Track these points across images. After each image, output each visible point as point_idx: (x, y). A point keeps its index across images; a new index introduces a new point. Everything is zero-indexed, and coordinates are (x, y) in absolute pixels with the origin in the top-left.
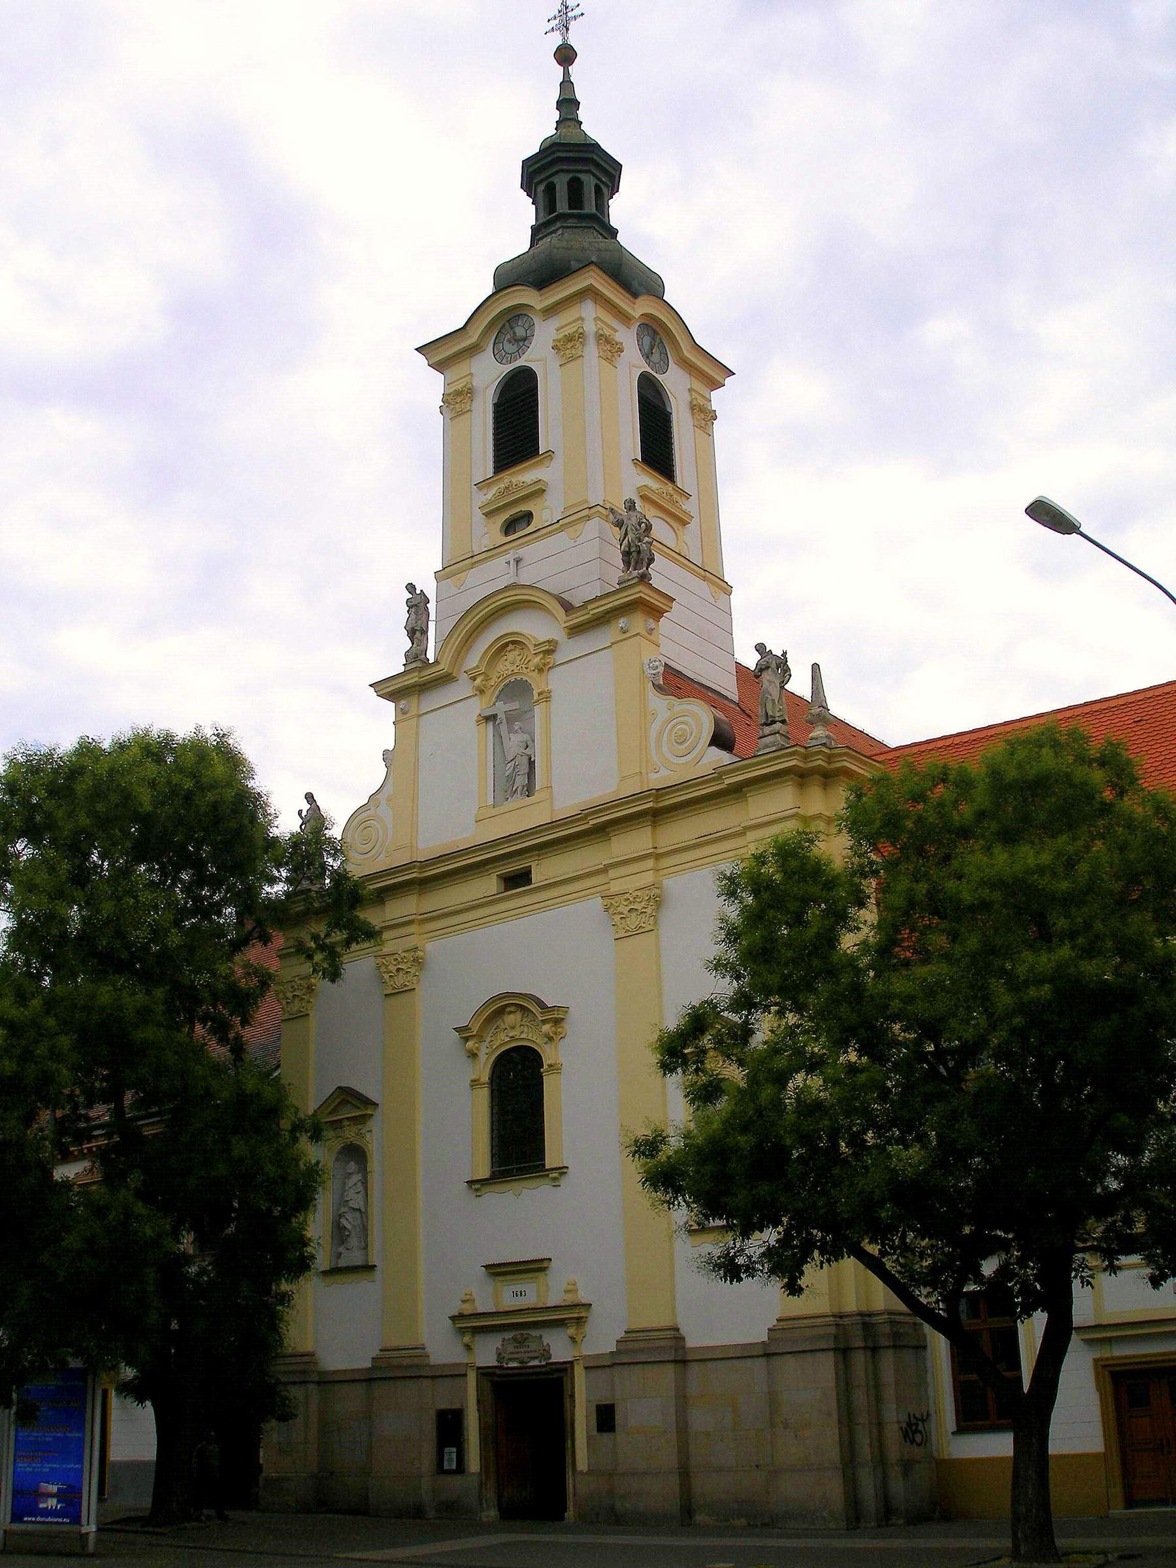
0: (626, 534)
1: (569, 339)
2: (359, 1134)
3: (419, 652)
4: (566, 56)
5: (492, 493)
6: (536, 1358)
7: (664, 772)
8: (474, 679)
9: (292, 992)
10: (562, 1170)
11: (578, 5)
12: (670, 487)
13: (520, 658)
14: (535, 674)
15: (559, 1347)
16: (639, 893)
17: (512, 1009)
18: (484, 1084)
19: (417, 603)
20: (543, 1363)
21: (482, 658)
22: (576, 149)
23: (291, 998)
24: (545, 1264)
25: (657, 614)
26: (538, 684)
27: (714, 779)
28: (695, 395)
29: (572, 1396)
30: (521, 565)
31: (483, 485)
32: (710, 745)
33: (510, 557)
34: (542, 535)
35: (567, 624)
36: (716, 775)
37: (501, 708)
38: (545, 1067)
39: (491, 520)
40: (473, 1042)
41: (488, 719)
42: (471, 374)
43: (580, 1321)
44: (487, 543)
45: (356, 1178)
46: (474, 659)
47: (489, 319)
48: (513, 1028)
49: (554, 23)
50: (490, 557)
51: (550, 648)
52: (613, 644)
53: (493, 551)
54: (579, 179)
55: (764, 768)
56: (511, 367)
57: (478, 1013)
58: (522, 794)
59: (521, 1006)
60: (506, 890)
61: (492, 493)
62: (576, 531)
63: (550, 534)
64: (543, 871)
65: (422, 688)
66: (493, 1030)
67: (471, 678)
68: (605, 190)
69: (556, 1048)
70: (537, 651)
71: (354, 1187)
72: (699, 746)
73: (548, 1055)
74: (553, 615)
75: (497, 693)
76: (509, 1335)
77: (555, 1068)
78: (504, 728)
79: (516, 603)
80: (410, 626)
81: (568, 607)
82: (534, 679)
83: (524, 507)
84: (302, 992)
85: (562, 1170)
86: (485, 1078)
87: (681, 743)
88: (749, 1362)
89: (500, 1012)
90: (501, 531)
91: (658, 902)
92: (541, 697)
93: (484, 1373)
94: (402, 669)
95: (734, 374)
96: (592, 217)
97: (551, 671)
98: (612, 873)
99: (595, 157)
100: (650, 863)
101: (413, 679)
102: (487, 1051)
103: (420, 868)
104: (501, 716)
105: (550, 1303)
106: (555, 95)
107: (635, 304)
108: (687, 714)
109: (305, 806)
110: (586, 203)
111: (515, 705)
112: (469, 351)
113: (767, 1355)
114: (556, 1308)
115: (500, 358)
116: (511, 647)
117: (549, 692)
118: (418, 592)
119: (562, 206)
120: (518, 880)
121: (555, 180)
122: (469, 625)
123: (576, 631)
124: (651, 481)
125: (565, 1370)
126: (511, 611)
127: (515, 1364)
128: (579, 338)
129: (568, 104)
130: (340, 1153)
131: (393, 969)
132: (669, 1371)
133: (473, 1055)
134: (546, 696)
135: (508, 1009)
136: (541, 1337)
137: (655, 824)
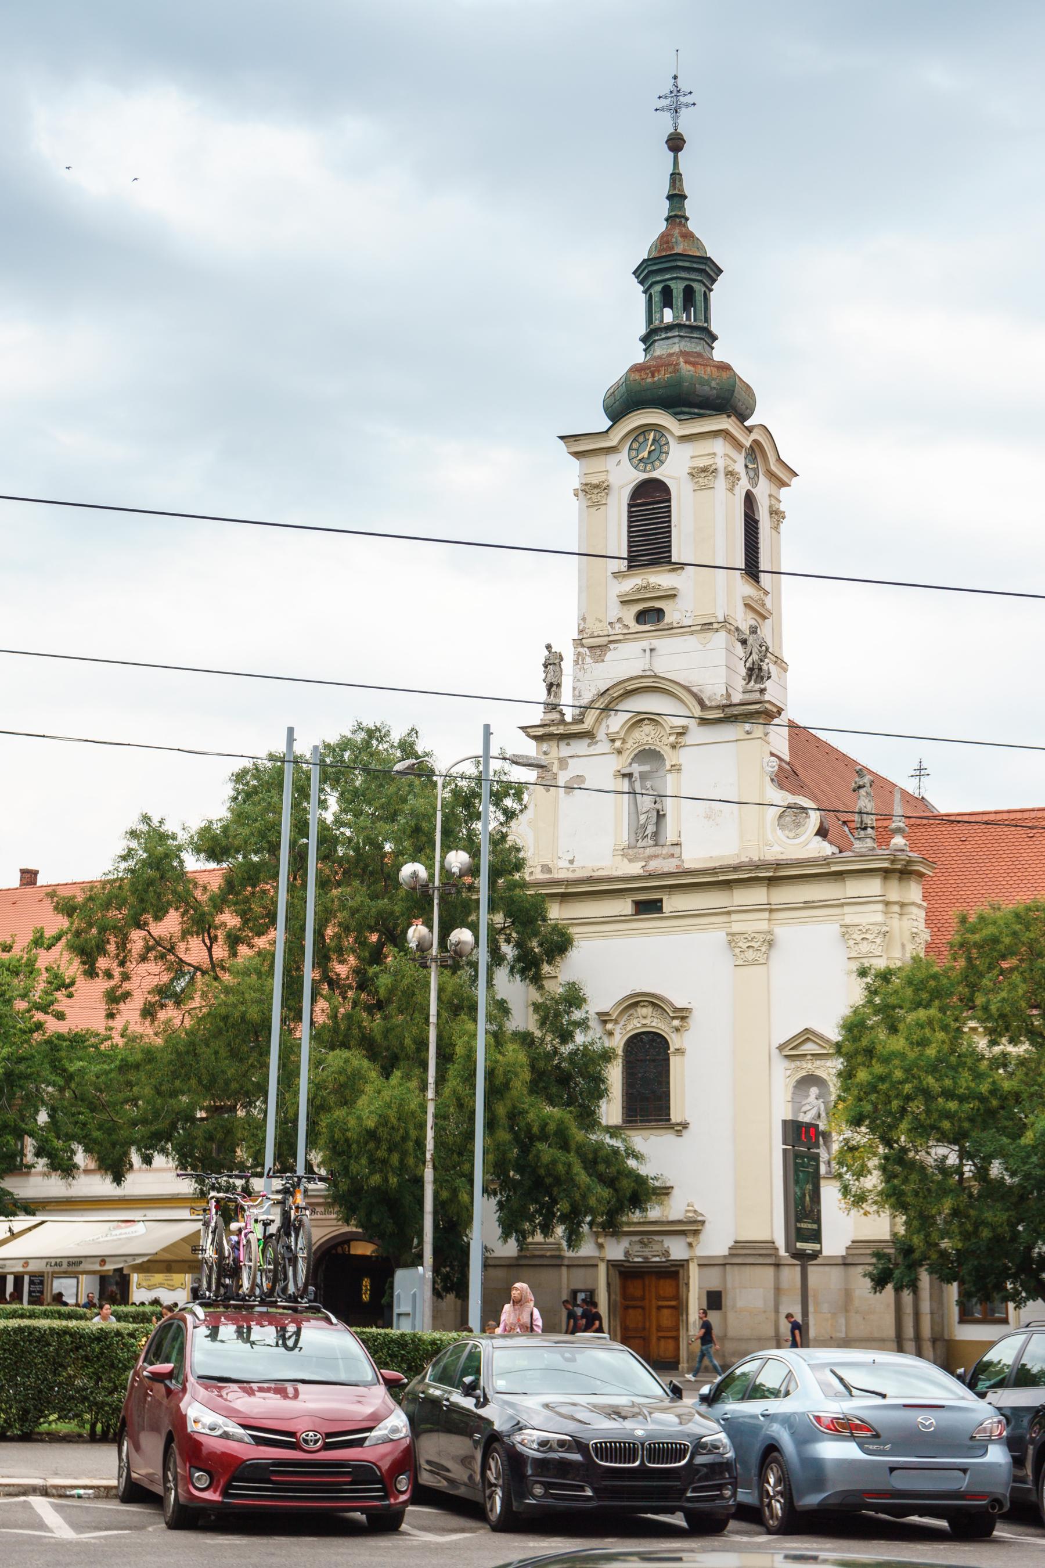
0: (751, 653)
1: (704, 470)
4: (676, 143)
6: (658, 1256)
8: (613, 741)
10: (685, 1126)
13: (654, 732)
14: (668, 748)
15: (677, 1249)
16: (871, 927)
17: (646, 1004)
19: (552, 662)
20: (664, 1260)
21: (623, 726)
24: (670, 1190)
26: (671, 758)
29: (687, 1284)
30: (654, 653)
33: (645, 644)
37: (636, 769)
38: (672, 1049)
39: (626, 608)
43: (696, 1233)
46: (616, 722)
48: (645, 1017)
49: (665, 102)
51: (682, 732)
57: (620, 1003)
62: (705, 638)
64: (672, 903)
66: (626, 1016)
69: (681, 1036)
73: (675, 1042)
75: (632, 756)
76: (636, 1238)
77: (679, 1051)
82: (666, 751)
83: (657, 604)
85: (685, 1126)
88: (827, 1268)
89: (636, 1004)
91: (770, 944)
92: (673, 768)
93: (612, 1264)
98: (734, 917)
99: (708, 269)
100: (766, 915)
102: (621, 1031)
103: (566, 885)
104: (636, 775)
105: (671, 1218)
106: (665, 189)
111: (646, 768)
113: (845, 1264)
114: (679, 1222)
116: (646, 722)
117: (680, 765)
120: (648, 907)
121: (673, 284)
123: (704, 722)
125: (682, 1266)
127: (640, 1260)
128: (713, 472)
129: (677, 198)
132: (770, 1271)
134: (676, 768)
135: (642, 1004)
136: (662, 1241)
137: (769, 886)
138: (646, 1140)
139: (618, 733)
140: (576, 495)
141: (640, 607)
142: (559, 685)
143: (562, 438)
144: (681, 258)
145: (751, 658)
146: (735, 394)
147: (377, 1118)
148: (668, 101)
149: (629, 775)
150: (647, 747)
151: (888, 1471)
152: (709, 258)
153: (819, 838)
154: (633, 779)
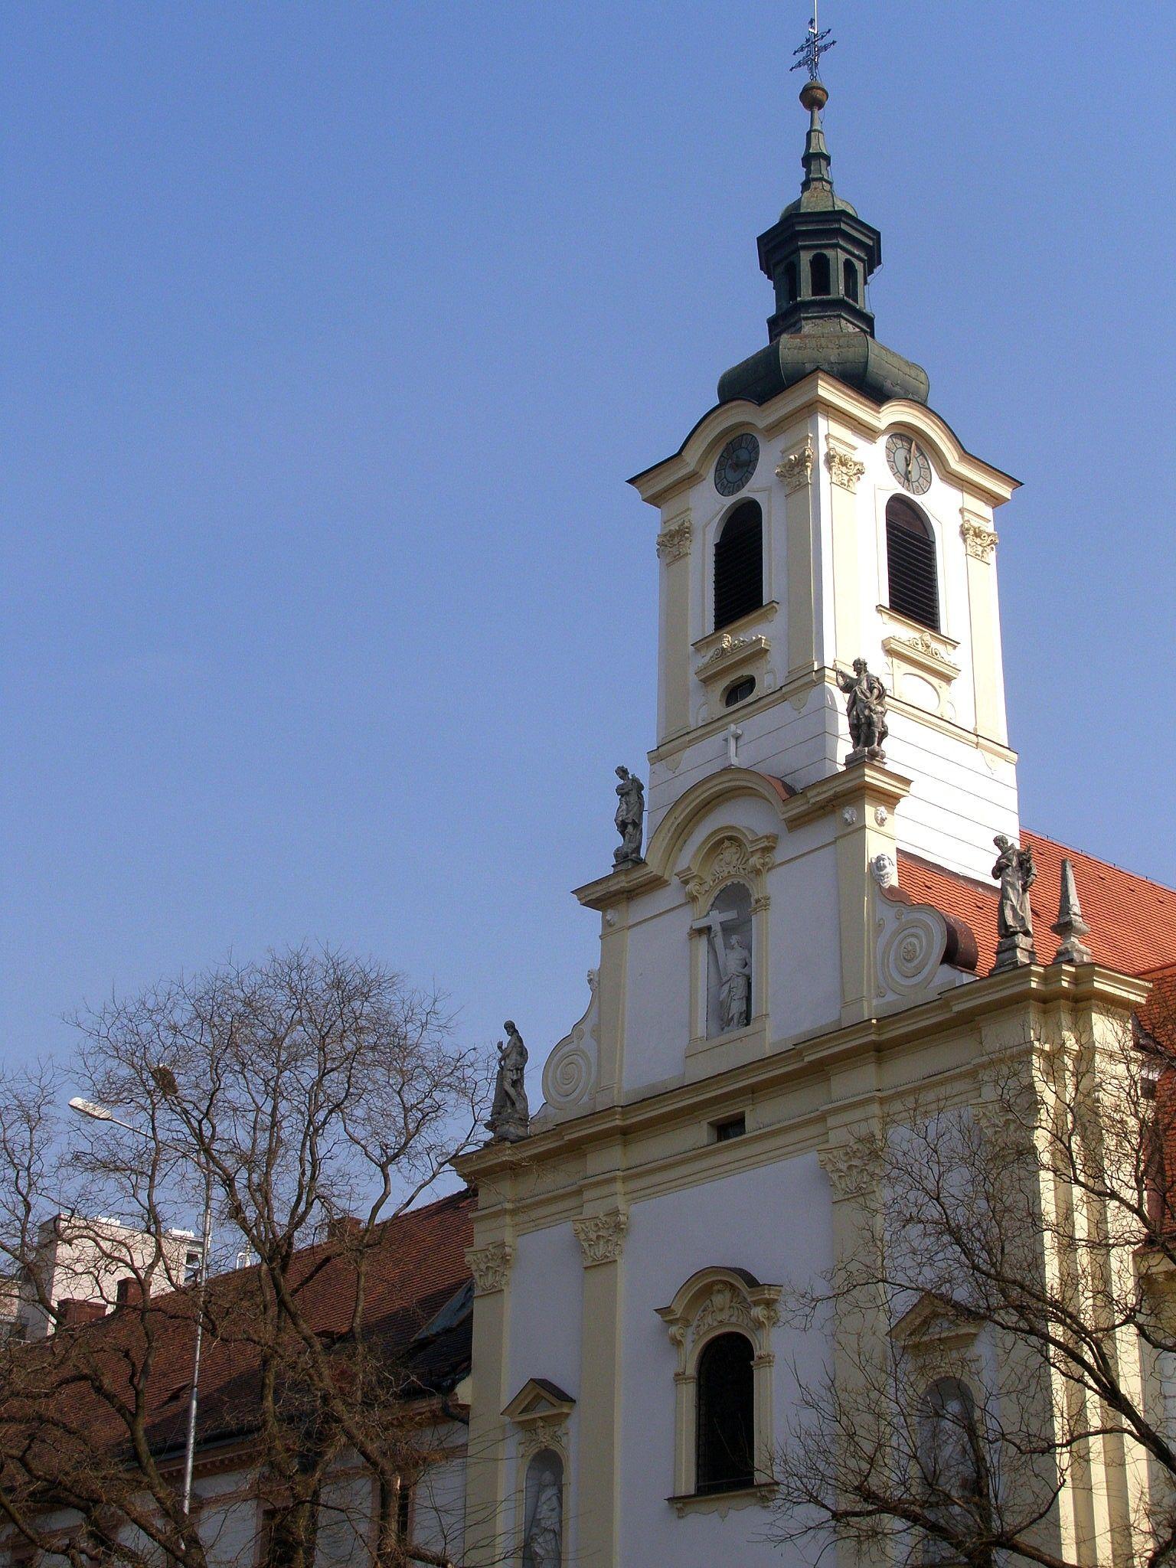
2: (556, 1438)
4: (812, 99)
7: (891, 997)
8: (686, 882)
9: (486, 1263)
11: (829, 31)
12: (927, 635)
18: (690, 1378)
19: (630, 789)
22: (815, 219)
23: (484, 1270)
27: (940, 1007)
28: (967, 516)
30: (741, 743)
31: (700, 645)
32: (943, 962)
34: (765, 706)
35: (784, 817)
36: (940, 1002)
37: (716, 918)
40: (677, 1327)
45: (550, 1492)
48: (721, 1310)
49: (801, 56)
50: (708, 733)
53: (711, 726)
54: (824, 256)
56: (729, 501)
58: (739, 1022)
59: (732, 1285)
60: (720, 1139)
63: (774, 704)
65: (630, 895)
67: (682, 882)
68: (859, 266)
70: (755, 848)
71: (548, 1503)
72: (931, 963)
74: (768, 800)
75: (712, 899)
78: (719, 941)
79: (732, 790)
80: (620, 819)
81: (791, 791)
83: (745, 672)
84: (496, 1264)
86: (691, 1370)
87: (909, 961)
89: (706, 1292)
94: (611, 871)
95: (1022, 484)
96: (839, 304)
99: (843, 226)
101: (623, 882)
103: (622, 1114)
104: (717, 928)
107: (879, 413)
108: (914, 924)
109: (506, 1039)
115: (725, 487)
116: (727, 843)
119: (806, 294)
120: (729, 1128)
122: (681, 815)
123: (795, 823)
124: (905, 632)
126: (728, 800)
130: (534, 1460)
131: (593, 1236)
133: (677, 1343)
135: (716, 1288)
138: (723, 1517)
139: (689, 869)
141: (725, 682)
142: (637, 825)
143: (631, 481)
144: (803, 220)
145: (855, 709)
146: (870, 368)
147: (253, 1503)
148: (804, 54)
152: (843, 213)
153: (946, 967)
154: (712, 935)
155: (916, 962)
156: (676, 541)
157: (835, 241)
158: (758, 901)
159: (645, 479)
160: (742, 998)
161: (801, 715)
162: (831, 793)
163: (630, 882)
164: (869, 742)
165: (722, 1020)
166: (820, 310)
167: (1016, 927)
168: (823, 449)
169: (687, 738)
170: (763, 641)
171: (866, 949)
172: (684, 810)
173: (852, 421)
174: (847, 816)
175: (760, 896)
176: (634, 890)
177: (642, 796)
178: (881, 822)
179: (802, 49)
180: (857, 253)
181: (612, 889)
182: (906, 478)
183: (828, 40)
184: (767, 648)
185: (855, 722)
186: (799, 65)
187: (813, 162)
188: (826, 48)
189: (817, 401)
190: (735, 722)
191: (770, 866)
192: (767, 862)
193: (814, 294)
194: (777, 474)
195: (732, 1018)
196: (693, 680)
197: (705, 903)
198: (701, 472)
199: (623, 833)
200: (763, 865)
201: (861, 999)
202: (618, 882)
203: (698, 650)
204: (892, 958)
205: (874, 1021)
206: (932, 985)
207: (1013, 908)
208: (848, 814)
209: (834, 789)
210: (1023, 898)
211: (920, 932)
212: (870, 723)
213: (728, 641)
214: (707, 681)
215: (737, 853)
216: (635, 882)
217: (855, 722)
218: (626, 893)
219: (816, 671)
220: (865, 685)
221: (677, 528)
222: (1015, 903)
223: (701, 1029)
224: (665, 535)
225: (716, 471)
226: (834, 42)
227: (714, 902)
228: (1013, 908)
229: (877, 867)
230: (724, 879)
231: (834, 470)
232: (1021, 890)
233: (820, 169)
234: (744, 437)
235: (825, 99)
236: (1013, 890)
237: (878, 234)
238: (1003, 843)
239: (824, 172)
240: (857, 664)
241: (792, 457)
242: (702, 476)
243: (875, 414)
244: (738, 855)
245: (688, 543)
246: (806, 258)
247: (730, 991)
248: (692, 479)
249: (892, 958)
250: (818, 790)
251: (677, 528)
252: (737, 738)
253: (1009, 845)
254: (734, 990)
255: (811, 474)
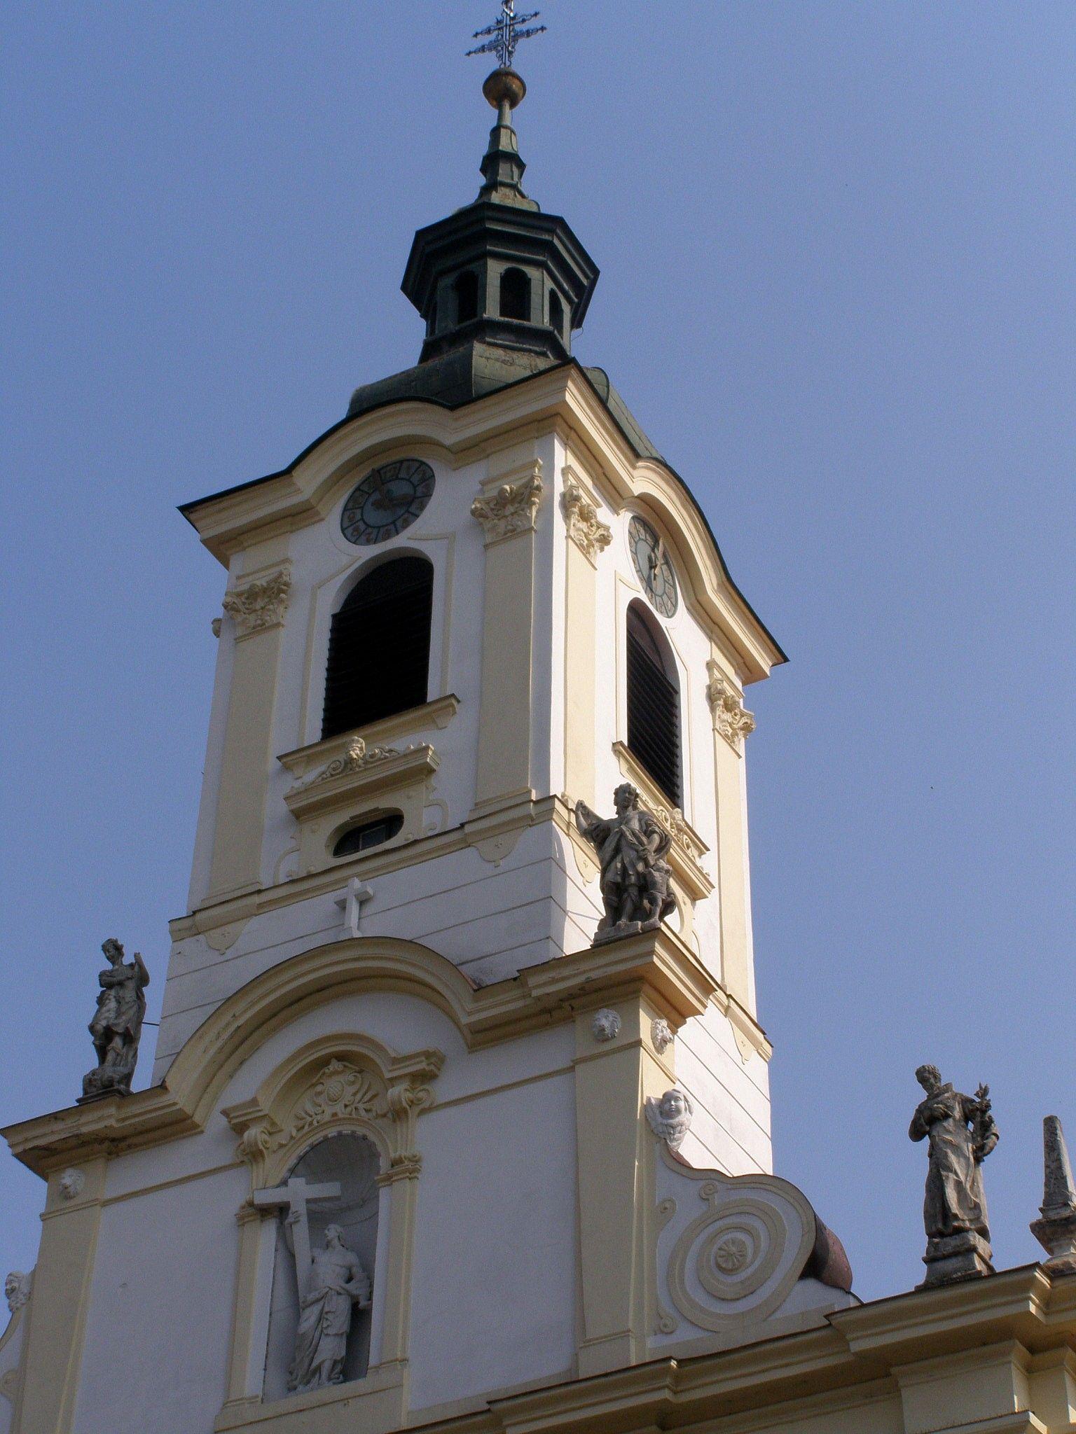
3: (117, 1077)
5: (311, 775)
13: (352, 1089)
25: (675, 1016)
26: (390, 1147)
30: (370, 908)
31: (287, 760)
32: (804, 1276)
37: (300, 1192)
41: (264, 1211)
42: (286, 561)
44: (291, 866)
47: (346, 457)
49: (486, 39)
52: (577, 1062)
54: (523, 274)
55: (952, 1317)
56: (369, 552)
61: (311, 775)
75: (292, 1161)
78: (301, 1233)
80: (104, 1023)
83: (386, 802)
90: (327, 846)
92: (397, 1169)
97: (425, 1118)
99: (556, 241)
106: (481, 54)
110: (534, 313)
111: (330, 1189)
112: (289, 519)
115: (355, 529)
117: (415, 1160)
118: (128, 959)
119: (492, 310)
122: (246, 1013)
139: (254, 1102)
140: (217, 633)
142: (130, 1039)
143: (186, 509)
144: (499, 215)
145: (619, 858)
148: (492, 37)
149: (281, 1211)
150: (332, 1132)
151: (460, 704)
154: (290, 1219)
155: (744, 1275)
156: (259, 604)
157: (541, 258)
158: (395, 1163)
159: (218, 507)
160: (342, 1334)
161: (498, 871)
162: (580, 979)
163: (124, 1120)
164: (640, 913)
165: (291, 1373)
166: (514, 338)
167: (963, 1220)
168: (559, 487)
169: (257, 899)
170: (430, 753)
171: (634, 1253)
172: (253, 1004)
173: (597, 466)
174: (605, 1023)
175: (403, 1153)
176: (124, 1138)
177: (143, 995)
178: (661, 1045)
179: (489, 31)
180: (566, 286)
181: (85, 1130)
182: (648, 583)
183: (532, 24)
184: (435, 767)
185: (619, 879)
186: (483, 49)
187: (501, 164)
188: (528, 33)
189: (557, 414)
190: (363, 876)
191: (426, 1105)
192: (419, 1100)
193: (502, 315)
194: (473, 512)
195: (318, 1369)
196: (275, 807)
197: (274, 1167)
198: (319, 508)
199: (102, 1052)
200: (412, 1103)
201: (626, 1334)
202: (100, 1119)
203: (287, 768)
204: (690, 1265)
205: (673, 1363)
206: (778, 1315)
207: (959, 1184)
208: (607, 1020)
209: (586, 975)
210: (975, 1173)
211: (757, 1224)
212: (646, 886)
213: (361, 749)
214: (301, 815)
215: (353, 1083)
216: (133, 1121)
217: (619, 879)
218: (107, 1144)
219: (536, 803)
220: (635, 825)
221: (265, 584)
222: (962, 1178)
223: (252, 1380)
224: (239, 595)
225: (345, 510)
226: (543, 29)
227: (307, 1153)
228: (959, 1184)
229: (661, 1113)
230: (322, 1126)
231: (573, 521)
232: (972, 1157)
233: (505, 172)
234: (405, 465)
235: (521, 95)
236: (958, 1156)
237: (596, 272)
238: (935, 1077)
239: (516, 179)
240: (625, 792)
241: (507, 487)
242: (318, 513)
243: (629, 467)
244: (357, 1086)
245: (281, 608)
246: (495, 270)
247: (320, 1320)
248: (301, 516)
249: (690, 1265)
250: (552, 974)
251: (265, 584)
252: (363, 902)
253: (943, 1083)
254: (330, 1317)
255: (536, 517)
